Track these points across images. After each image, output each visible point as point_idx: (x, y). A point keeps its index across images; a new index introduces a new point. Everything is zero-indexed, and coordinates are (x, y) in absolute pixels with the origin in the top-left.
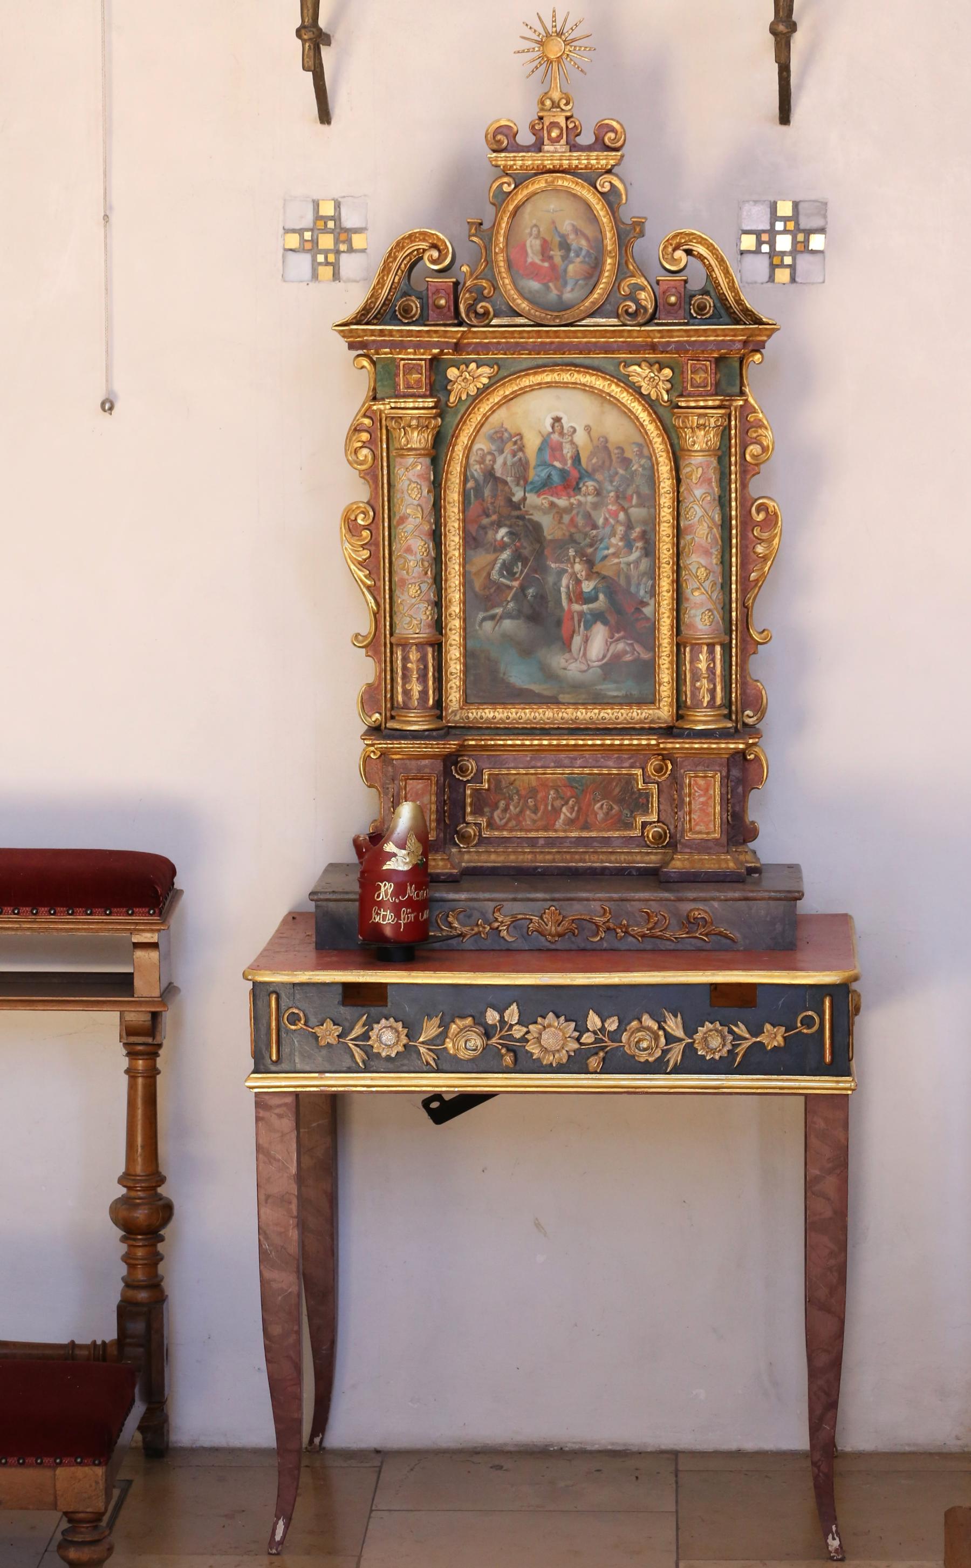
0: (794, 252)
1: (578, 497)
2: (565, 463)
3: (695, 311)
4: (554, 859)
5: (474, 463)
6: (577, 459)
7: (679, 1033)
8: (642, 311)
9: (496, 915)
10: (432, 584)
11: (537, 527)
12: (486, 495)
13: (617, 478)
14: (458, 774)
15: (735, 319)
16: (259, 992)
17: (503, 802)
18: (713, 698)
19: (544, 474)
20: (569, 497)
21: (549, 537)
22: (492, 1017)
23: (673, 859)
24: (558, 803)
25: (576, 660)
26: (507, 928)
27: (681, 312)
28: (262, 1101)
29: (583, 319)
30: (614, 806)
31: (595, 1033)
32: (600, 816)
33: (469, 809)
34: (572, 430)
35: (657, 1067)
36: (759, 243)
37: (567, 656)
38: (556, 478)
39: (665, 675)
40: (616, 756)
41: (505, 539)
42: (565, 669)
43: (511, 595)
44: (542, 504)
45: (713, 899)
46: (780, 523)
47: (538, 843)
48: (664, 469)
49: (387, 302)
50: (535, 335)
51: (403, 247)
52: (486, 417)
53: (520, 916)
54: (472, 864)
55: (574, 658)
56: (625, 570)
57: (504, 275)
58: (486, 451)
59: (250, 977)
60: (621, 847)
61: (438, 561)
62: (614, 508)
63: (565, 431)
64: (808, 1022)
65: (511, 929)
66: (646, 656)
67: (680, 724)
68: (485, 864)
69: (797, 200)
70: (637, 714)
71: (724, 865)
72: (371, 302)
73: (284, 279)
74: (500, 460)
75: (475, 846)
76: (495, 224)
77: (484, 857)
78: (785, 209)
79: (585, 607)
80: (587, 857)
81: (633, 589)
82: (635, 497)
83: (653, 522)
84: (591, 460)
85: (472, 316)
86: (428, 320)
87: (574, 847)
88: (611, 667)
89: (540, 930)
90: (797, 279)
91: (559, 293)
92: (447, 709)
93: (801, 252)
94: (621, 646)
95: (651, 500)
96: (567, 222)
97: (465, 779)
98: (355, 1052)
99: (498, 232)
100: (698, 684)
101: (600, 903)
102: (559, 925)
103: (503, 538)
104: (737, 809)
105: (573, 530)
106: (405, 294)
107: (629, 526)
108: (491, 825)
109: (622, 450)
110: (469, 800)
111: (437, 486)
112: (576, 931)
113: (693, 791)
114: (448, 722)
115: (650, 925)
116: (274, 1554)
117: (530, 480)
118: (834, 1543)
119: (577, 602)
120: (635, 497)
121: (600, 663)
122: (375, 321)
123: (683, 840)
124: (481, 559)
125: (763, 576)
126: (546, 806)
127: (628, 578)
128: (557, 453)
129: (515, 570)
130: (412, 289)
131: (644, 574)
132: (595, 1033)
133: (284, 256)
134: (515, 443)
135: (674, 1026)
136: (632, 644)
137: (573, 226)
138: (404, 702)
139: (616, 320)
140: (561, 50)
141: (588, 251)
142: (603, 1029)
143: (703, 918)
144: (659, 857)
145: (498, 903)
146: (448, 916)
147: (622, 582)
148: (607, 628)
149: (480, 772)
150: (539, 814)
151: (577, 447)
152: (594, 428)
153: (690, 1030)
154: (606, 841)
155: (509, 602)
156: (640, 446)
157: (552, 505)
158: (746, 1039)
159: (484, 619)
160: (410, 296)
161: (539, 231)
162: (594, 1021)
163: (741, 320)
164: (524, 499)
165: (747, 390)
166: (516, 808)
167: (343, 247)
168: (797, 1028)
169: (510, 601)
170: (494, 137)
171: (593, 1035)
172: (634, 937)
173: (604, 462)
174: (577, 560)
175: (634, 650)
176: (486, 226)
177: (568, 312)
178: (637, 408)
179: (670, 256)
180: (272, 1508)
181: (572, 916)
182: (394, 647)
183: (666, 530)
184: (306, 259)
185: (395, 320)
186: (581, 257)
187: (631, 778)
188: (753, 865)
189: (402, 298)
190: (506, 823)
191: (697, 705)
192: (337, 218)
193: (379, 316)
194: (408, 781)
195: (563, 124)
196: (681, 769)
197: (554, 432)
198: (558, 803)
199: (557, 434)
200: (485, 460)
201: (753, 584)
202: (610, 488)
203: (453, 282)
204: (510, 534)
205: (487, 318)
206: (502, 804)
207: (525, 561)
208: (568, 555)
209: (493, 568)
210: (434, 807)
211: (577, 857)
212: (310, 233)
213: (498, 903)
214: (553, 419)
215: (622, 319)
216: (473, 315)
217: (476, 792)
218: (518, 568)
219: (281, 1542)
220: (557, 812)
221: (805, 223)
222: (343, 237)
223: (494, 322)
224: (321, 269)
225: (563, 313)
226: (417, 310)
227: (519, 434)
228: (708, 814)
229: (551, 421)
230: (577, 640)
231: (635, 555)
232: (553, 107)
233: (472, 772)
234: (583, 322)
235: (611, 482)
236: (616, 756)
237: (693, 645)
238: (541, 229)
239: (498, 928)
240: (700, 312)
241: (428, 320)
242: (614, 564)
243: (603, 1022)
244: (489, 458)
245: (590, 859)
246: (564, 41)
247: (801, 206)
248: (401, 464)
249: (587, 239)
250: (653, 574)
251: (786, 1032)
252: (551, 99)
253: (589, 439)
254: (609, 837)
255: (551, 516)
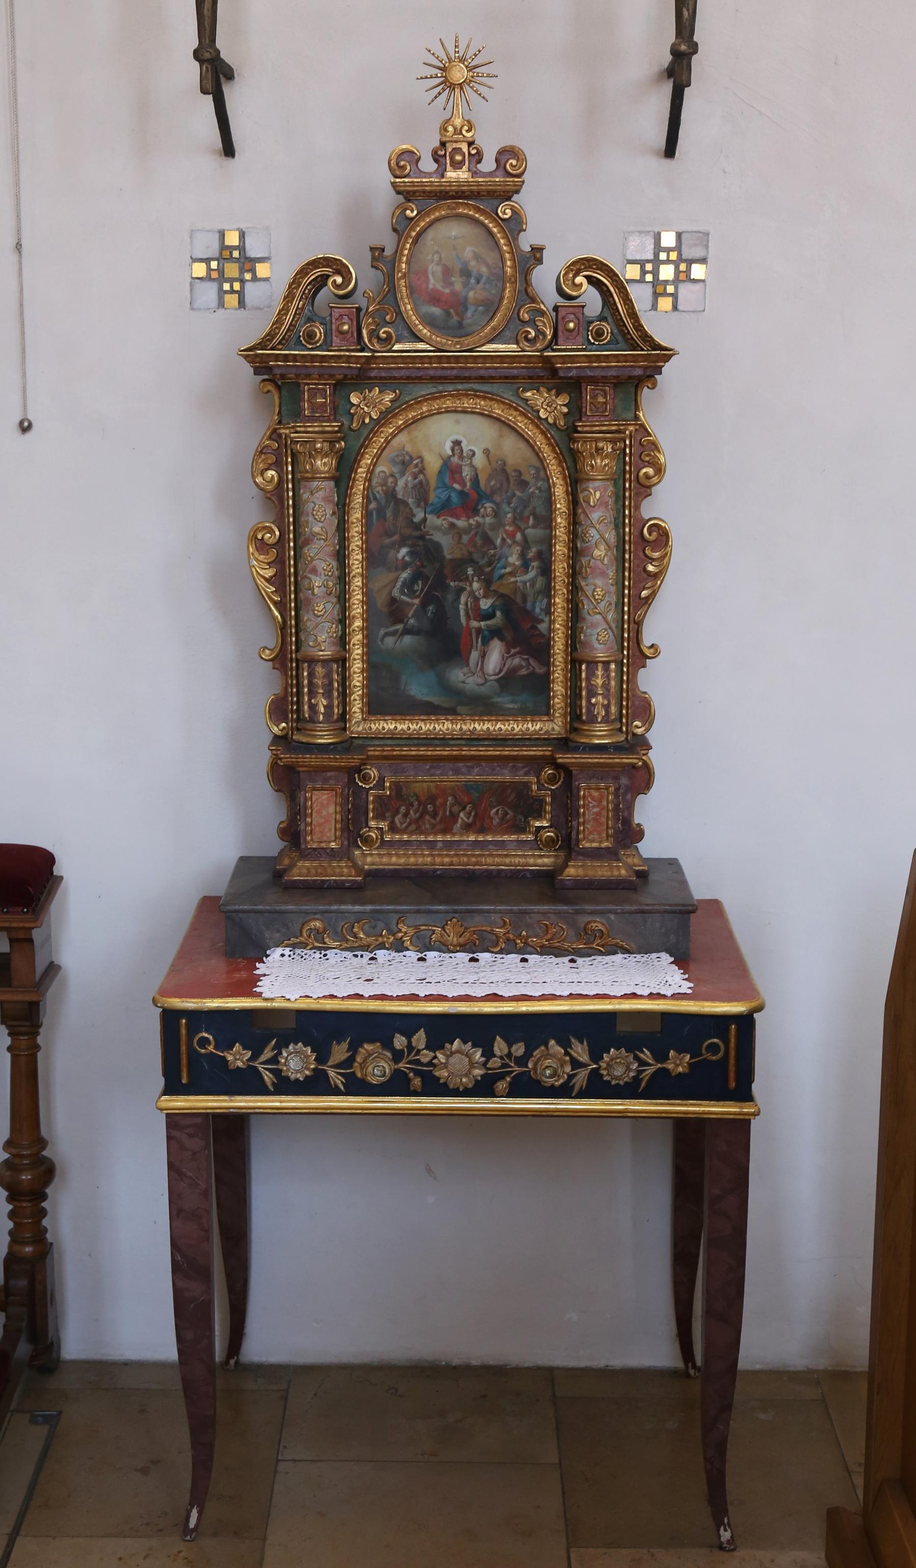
0: (676, 281)
1: (477, 518)
2: (464, 485)
3: (593, 338)
4: (452, 861)
5: (377, 485)
6: (475, 480)
7: (584, 1058)
8: (541, 337)
9: (400, 926)
10: (336, 604)
11: (437, 547)
12: (388, 516)
13: (514, 500)
14: (361, 782)
15: (632, 345)
16: (170, 1018)
17: (403, 807)
18: (608, 713)
19: (444, 496)
20: (469, 518)
21: (448, 557)
22: (399, 1042)
23: (567, 866)
24: (456, 809)
25: (474, 674)
26: (411, 939)
27: (580, 339)
28: (174, 1121)
29: (483, 345)
30: (509, 812)
31: (501, 1058)
32: (496, 821)
33: (371, 815)
34: (471, 453)
35: (564, 1091)
36: (644, 272)
37: (465, 670)
38: (455, 498)
39: (558, 688)
40: (511, 764)
41: (407, 558)
42: (463, 682)
43: (412, 612)
44: (442, 525)
45: (610, 911)
46: (670, 543)
47: (436, 846)
48: (559, 491)
49: (291, 328)
50: (436, 361)
51: (307, 274)
52: (388, 442)
53: (423, 928)
54: (374, 867)
55: (472, 673)
56: (521, 588)
57: (406, 301)
58: (388, 473)
59: (159, 1005)
60: (515, 850)
61: (343, 578)
62: (511, 529)
63: (465, 454)
64: (714, 1048)
65: (414, 939)
66: (540, 670)
67: (573, 736)
68: (387, 867)
69: (680, 231)
70: (534, 727)
71: (616, 873)
72: (276, 328)
73: (192, 309)
74: (401, 483)
75: (377, 848)
76: (398, 252)
77: (385, 860)
78: (669, 239)
79: (483, 624)
80: (483, 860)
81: (529, 606)
82: (531, 518)
83: (549, 541)
84: (489, 483)
85: (375, 341)
86: (331, 346)
87: (471, 850)
88: (507, 680)
89: (442, 940)
90: (679, 307)
91: (459, 319)
92: (350, 721)
93: (683, 281)
94: (517, 661)
95: (547, 522)
96: (469, 249)
97: (368, 787)
98: (264, 1075)
99: (400, 259)
100: (593, 700)
101: (500, 915)
102: (460, 936)
103: (404, 557)
104: (626, 814)
105: (472, 550)
106: (309, 320)
107: (526, 545)
108: (393, 829)
109: (520, 473)
110: (371, 807)
111: (342, 509)
112: (477, 942)
113: (587, 802)
114: (352, 733)
115: (549, 936)
116: (189, 1541)
117: (430, 502)
118: (726, 1535)
119: (475, 619)
120: (531, 518)
121: (497, 677)
122: (280, 347)
123: (576, 848)
124: (383, 577)
125: (653, 595)
126: (445, 811)
127: (524, 598)
128: (457, 476)
129: (416, 588)
130: (316, 315)
131: (539, 592)
132: (501, 1058)
133: (191, 285)
134: (416, 466)
135: (580, 1051)
136: (527, 660)
137: (474, 252)
138: (309, 716)
139: (515, 346)
140: (463, 77)
141: (488, 278)
142: (509, 1055)
143: (600, 930)
144: (552, 860)
145: (402, 915)
146: (353, 927)
147: (519, 600)
148: (504, 643)
149: (381, 780)
150: (438, 819)
151: (476, 469)
152: (492, 451)
153: (596, 1056)
154: (502, 844)
155: (409, 618)
156: (537, 468)
157: (452, 525)
158: (650, 1065)
159: (387, 634)
160: (314, 322)
161: (440, 258)
162: (500, 1046)
163: (638, 345)
164: (425, 520)
165: (641, 415)
166: (415, 814)
167: (248, 276)
168: (702, 1055)
169: (411, 618)
170: (397, 164)
171: (499, 1060)
172: (533, 947)
173: (502, 485)
174: (476, 579)
175: (530, 664)
176: (388, 252)
177: (469, 337)
178: (530, 431)
179: (570, 282)
180: (187, 1497)
181: (474, 927)
182: (300, 663)
183: (560, 549)
184: (212, 288)
185: (299, 344)
186: (481, 283)
187: (527, 785)
188: (641, 868)
189: (306, 324)
190: (407, 827)
191: (592, 719)
192: (241, 248)
193: (284, 342)
194: (314, 792)
195: (465, 149)
196: (577, 780)
197: (453, 455)
198: (456, 809)
199: (456, 457)
200: (387, 482)
201: (644, 601)
202: (508, 509)
203: (356, 308)
204: (410, 553)
205: (389, 344)
206: (403, 809)
207: (426, 579)
208: (466, 574)
209: (394, 586)
210: (339, 817)
211: (473, 859)
212: (216, 263)
213: (402, 915)
214: (452, 442)
215: (521, 345)
216: (376, 341)
217: (378, 798)
218: (418, 586)
219: (194, 1530)
220: (454, 817)
221: (687, 253)
222: (248, 266)
223: (396, 347)
224: (227, 297)
225: (464, 339)
226: (321, 336)
227: (420, 457)
228: (601, 824)
229: (451, 444)
230: (474, 655)
231: (532, 574)
232: (455, 134)
233: (374, 780)
234: (484, 348)
235: (509, 503)
236: (511, 764)
237: (589, 663)
238: (443, 256)
239: (401, 938)
240: (598, 338)
241: (331, 346)
242: (511, 583)
243: (510, 1046)
244: (390, 480)
245: (486, 862)
246: (467, 67)
247: (684, 236)
248: (305, 487)
249: (487, 265)
250: (548, 592)
251: (691, 1058)
252: (452, 126)
253: (487, 463)
254: (504, 841)
255: (451, 536)
